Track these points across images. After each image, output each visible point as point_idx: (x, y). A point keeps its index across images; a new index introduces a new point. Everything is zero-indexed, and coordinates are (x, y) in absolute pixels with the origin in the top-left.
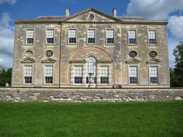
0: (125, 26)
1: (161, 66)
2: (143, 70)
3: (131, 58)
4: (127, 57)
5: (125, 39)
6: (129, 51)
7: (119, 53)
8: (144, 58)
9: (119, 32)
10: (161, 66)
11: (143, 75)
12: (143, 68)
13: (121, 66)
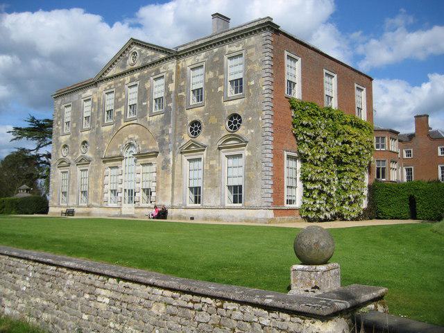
1: (250, 154)
2: (211, 167)
6: (189, 122)
10: (250, 154)
11: (210, 182)
13: (171, 162)
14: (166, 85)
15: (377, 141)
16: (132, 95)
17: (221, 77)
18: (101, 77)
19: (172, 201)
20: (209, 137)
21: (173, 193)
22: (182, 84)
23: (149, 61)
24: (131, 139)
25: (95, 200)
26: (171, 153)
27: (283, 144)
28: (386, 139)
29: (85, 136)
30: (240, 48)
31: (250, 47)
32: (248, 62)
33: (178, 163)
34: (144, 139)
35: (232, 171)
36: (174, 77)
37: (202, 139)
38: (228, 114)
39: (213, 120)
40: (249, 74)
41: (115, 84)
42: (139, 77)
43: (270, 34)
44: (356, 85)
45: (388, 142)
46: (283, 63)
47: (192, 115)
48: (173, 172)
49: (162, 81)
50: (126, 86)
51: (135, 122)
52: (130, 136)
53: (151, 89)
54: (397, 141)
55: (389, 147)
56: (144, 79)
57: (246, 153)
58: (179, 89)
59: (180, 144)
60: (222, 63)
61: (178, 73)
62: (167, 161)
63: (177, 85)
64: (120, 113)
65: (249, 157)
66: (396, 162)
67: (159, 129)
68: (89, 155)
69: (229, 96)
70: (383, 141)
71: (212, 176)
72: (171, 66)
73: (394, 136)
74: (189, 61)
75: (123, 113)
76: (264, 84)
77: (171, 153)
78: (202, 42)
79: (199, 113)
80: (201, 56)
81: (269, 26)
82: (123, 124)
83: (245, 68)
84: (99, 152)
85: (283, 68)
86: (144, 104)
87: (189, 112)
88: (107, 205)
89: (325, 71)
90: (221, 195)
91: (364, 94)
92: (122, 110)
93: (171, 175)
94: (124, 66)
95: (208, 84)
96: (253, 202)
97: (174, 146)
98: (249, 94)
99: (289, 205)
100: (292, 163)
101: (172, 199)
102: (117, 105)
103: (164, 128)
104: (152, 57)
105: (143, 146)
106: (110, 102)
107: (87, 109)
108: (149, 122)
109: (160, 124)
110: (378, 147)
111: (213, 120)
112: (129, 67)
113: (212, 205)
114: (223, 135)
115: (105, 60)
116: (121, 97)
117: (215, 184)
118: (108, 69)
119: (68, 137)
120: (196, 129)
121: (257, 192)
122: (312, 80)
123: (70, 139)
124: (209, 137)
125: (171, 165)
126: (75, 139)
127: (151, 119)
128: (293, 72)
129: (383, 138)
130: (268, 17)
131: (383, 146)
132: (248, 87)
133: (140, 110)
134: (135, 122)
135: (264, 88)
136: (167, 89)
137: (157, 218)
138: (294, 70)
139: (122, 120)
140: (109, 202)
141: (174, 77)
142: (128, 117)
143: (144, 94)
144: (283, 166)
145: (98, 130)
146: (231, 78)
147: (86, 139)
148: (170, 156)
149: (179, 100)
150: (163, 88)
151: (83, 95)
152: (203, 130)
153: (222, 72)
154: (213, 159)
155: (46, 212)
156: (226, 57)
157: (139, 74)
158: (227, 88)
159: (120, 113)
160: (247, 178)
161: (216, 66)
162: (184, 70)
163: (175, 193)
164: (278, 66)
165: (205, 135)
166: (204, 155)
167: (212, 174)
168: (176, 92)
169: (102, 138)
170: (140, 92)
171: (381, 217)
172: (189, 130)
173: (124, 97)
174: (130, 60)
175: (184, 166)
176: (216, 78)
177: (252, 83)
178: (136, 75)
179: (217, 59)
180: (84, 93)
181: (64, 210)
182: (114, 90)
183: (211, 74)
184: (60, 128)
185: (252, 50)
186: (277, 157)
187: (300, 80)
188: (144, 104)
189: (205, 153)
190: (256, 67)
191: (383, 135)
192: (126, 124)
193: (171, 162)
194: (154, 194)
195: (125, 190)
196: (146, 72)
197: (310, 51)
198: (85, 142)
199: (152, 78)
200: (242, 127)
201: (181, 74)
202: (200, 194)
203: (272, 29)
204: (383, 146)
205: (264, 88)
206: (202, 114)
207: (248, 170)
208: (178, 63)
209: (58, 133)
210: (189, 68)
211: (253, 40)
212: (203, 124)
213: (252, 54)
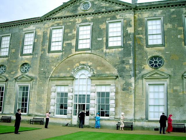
0: (140, 14)
1: (87, 74)
3: (151, 69)
4: (144, 68)
5: (141, 36)
6: (149, 57)
7: (129, 61)
8: (177, 68)
9: (130, 25)
12: (175, 88)
13: (133, 85)
14: (124, 28)
18: (48, 16)
20: (172, 69)
34: (99, 66)
36: (132, 23)
42: (92, 19)
52: (82, 62)
62: (128, 84)
86: (98, 39)
88: (54, 116)
93: (133, 96)
94: (76, 10)
103: (124, 59)
104: (106, 7)
108: (106, 53)
115: (138, 3)
118: (57, 11)
119: (6, 59)
123: (8, 60)
124: (172, 69)
125: (133, 88)
126: (14, 61)
127: (108, 51)
151: (25, 29)
154: (176, 85)
168: (134, 35)
170: (93, 30)
180: (25, 27)
188: (98, 39)
193: (133, 85)
206: (162, 52)
208: (134, 14)
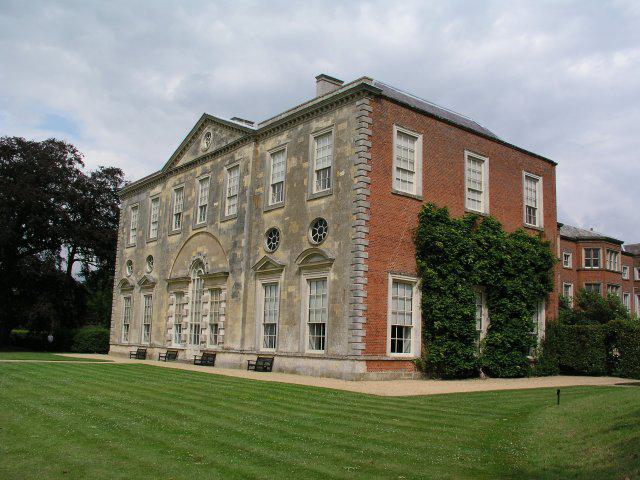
2: (290, 295)
14: (241, 177)
15: (587, 255)
16: (202, 193)
17: (305, 165)
19: (242, 343)
21: (243, 332)
22: (261, 175)
23: (224, 144)
24: (200, 254)
25: (157, 339)
26: (243, 274)
27: (385, 262)
28: (601, 251)
29: (151, 249)
30: (330, 123)
31: (342, 121)
32: (339, 143)
33: (251, 287)
34: (214, 255)
35: (310, 301)
36: (250, 166)
37: (281, 256)
38: (311, 218)
39: (294, 228)
40: (339, 159)
41: (186, 177)
43: (367, 102)
44: (524, 174)
45: (604, 256)
46: (390, 143)
47: (270, 220)
48: (245, 302)
49: (236, 174)
50: (197, 181)
51: (204, 229)
52: (200, 249)
53: (224, 184)
54: (619, 255)
55: (604, 263)
56: (217, 170)
57: (331, 276)
58: (257, 183)
59: (254, 261)
60: (307, 146)
61: (255, 160)
63: (254, 177)
64: (188, 216)
65: (334, 282)
66: (617, 287)
67: (230, 241)
68: (154, 275)
69: (315, 192)
70: (596, 255)
71: (290, 306)
72: (248, 151)
73: (612, 247)
74: (270, 144)
75: (191, 217)
76: (358, 176)
77: (243, 274)
78: (287, 115)
79: (277, 218)
80: (283, 138)
81: (366, 91)
82: (192, 233)
83: (335, 152)
84: (164, 272)
85: (390, 150)
87: (266, 216)
89: (467, 153)
90: (298, 336)
91: (539, 185)
92: (190, 212)
94: (196, 152)
95: (290, 176)
96: (340, 348)
97: (248, 264)
98: (338, 190)
99: (396, 355)
100: (402, 292)
101: (243, 340)
102: (186, 208)
105: (213, 264)
106: (177, 205)
107: (154, 211)
109: (232, 233)
110: (588, 264)
111: (294, 228)
112: (201, 154)
113: (289, 349)
114: (305, 249)
116: (190, 195)
117: (293, 321)
120: (320, 231)
121: (345, 334)
122: (442, 171)
128: (409, 156)
129: (596, 251)
130: (365, 78)
131: (596, 264)
132: (338, 179)
133: (212, 212)
134: (204, 229)
135: (356, 181)
136: (241, 183)
137: (201, 364)
138: (409, 153)
139: (191, 227)
140: (173, 341)
141: (250, 166)
142: (198, 223)
143: (216, 192)
144: (385, 295)
145: (164, 240)
146: (317, 167)
147: (151, 252)
148: (242, 279)
149: (255, 198)
150: (236, 183)
152: (282, 242)
153: (306, 159)
155: (106, 351)
156: (312, 137)
157: (211, 163)
158: (312, 179)
159: (188, 216)
160: (332, 313)
161: (301, 151)
162: (263, 156)
163: (247, 331)
164: (381, 148)
165: (284, 249)
166: (282, 279)
167: (290, 305)
169: (168, 252)
170: (211, 189)
171: (317, 393)
172: (311, 233)
173: (193, 195)
174: (204, 145)
175: (259, 293)
176: (299, 168)
177: (342, 174)
178: (208, 165)
179: (302, 139)
181: (134, 350)
182: (183, 185)
183: (294, 162)
184: (126, 237)
185: (344, 125)
186: (376, 282)
187: (421, 167)
189: (283, 274)
190: (348, 150)
191: (595, 246)
192: (195, 232)
194: (222, 332)
195: (191, 325)
196: (219, 160)
197: (440, 124)
198: (150, 258)
199: (225, 169)
200: (329, 238)
201: (259, 162)
202: (324, 334)
203: (370, 94)
204: (596, 264)
205: (356, 181)
207: (334, 301)
209: (122, 245)
210: (268, 154)
211: (345, 112)
212: (281, 234)
213: (343, 131)
